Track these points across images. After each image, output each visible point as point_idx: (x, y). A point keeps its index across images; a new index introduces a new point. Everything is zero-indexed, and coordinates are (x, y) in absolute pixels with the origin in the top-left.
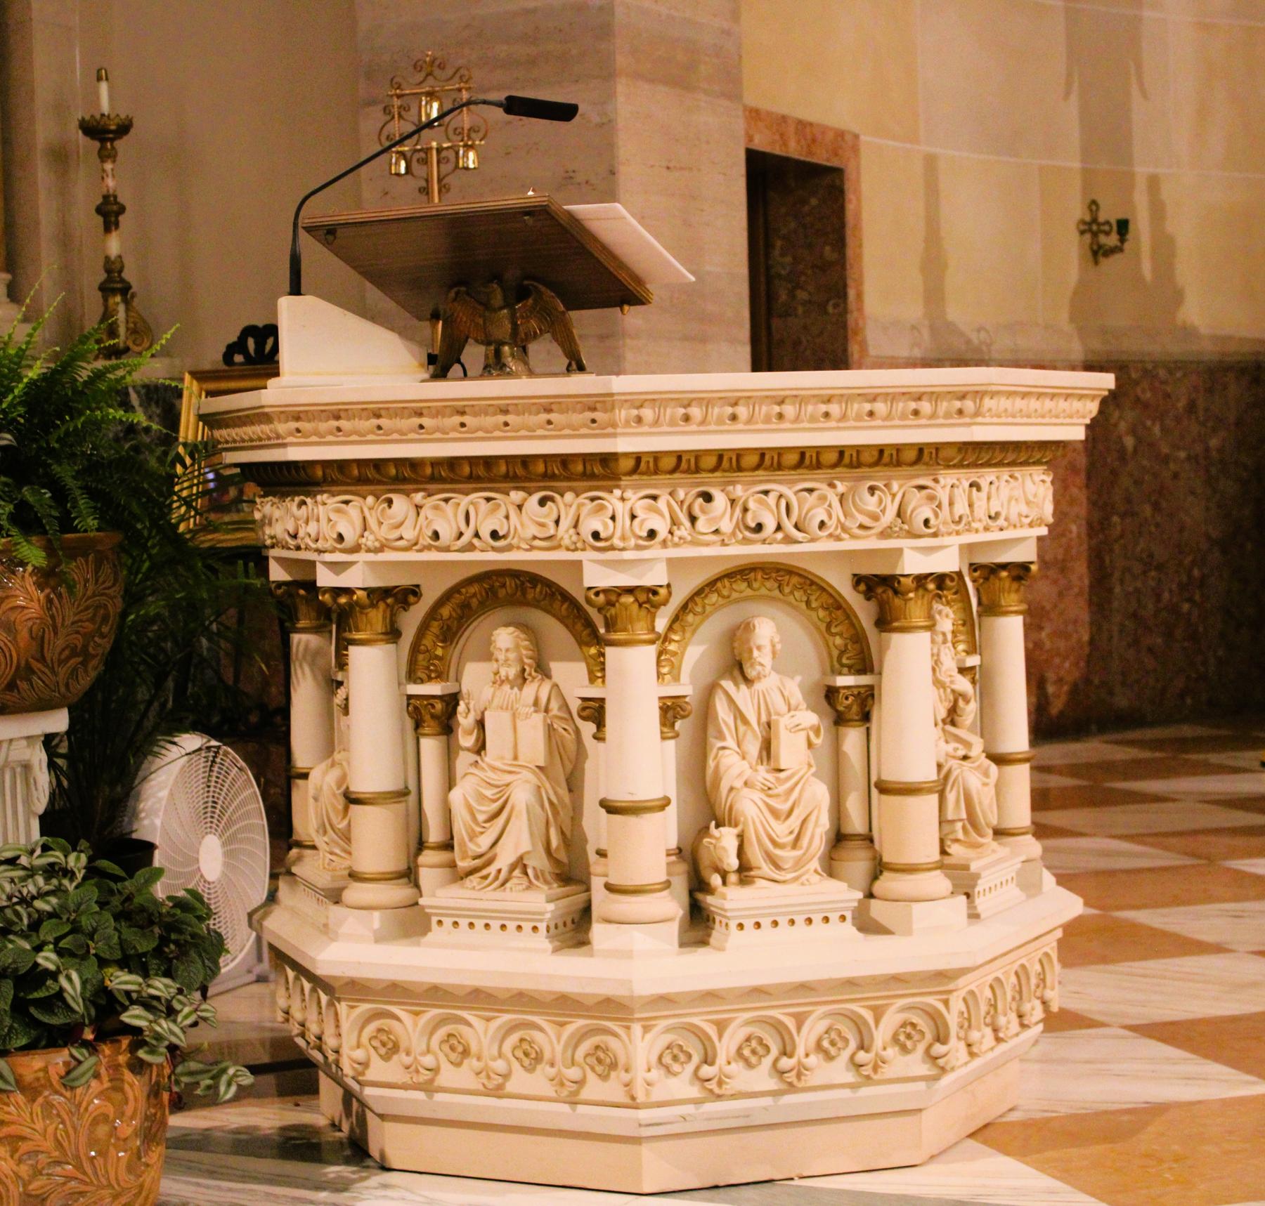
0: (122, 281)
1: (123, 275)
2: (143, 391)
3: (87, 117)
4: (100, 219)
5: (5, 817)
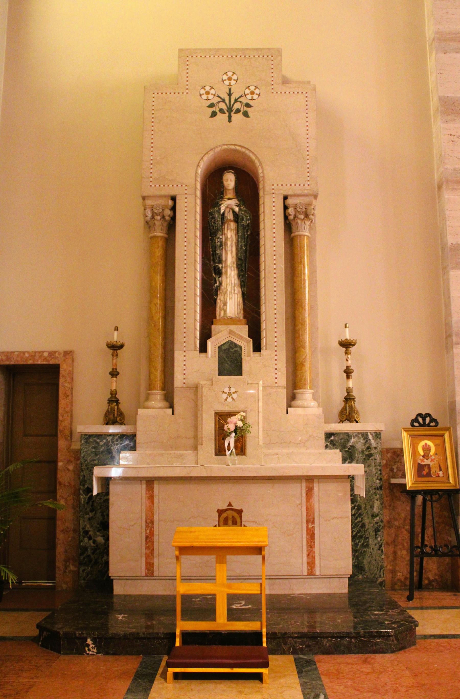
0: (116, 398)
1: (117, 396)
2: (374, 434)
3: (109, 342)
4: (345, 374)
5: (274, 576)
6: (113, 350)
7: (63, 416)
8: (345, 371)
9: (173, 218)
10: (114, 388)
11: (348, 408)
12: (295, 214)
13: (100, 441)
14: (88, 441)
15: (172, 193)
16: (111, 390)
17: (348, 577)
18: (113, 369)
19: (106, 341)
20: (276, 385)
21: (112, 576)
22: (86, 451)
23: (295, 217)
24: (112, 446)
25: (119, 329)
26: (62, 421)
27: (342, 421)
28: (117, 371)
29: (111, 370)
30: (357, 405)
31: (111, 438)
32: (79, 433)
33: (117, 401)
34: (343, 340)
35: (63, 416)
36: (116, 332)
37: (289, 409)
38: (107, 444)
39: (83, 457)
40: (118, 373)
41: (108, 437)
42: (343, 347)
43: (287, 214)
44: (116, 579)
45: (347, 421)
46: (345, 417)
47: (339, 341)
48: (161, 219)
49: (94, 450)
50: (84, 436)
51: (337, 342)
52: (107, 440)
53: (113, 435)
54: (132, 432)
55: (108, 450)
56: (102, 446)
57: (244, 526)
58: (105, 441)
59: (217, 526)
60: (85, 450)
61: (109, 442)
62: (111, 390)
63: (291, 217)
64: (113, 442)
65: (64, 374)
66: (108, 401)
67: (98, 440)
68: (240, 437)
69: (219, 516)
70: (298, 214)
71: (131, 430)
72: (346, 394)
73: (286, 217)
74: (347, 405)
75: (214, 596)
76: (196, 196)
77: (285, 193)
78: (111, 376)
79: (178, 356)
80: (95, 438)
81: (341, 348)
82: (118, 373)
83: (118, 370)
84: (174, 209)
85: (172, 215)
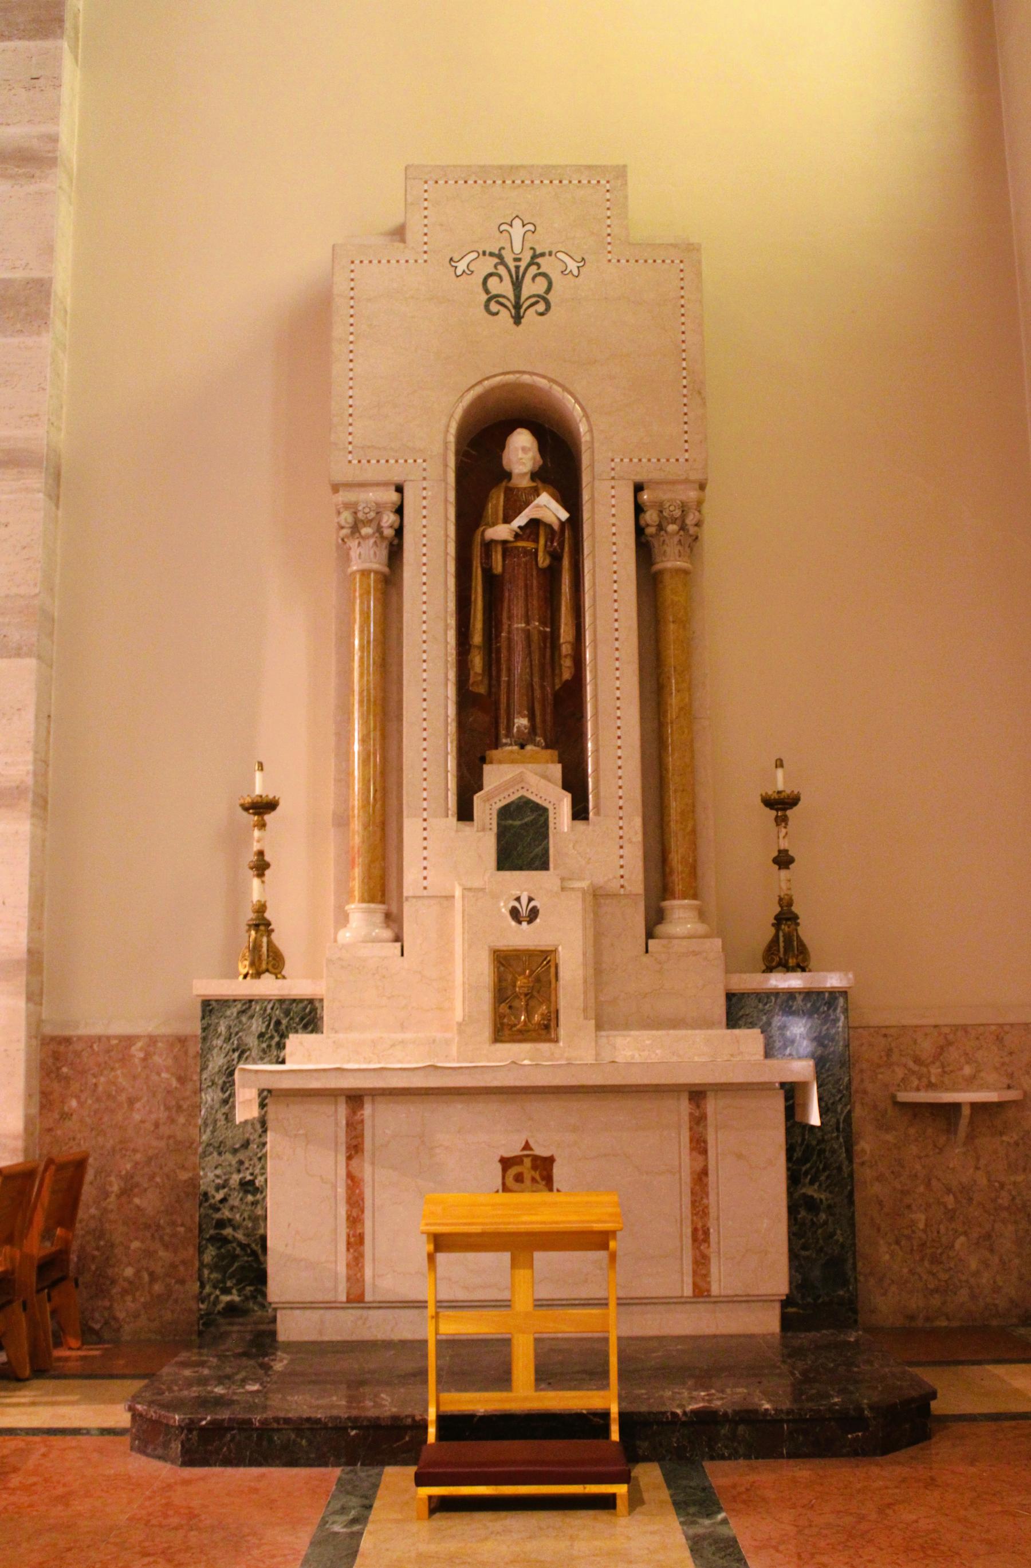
8: (267, 866)
9: (399, 532)
11: (781, 939)
12: (660, 522)
15: (397, 479)
16: (779, 896)
17: (782, 1301)
19: (759, 793)
20: (622, 891)
23: (660, 527)
25: (784, 763)
27: (769, 969)
30: (807, 931)
32: (198, 996)
33: (794, 918)
34: (770, 793)
37: (651, 942)
40: (791, 860)
42: (772, 808)
43: (642, 523)
46: (777, 959)
48: (374, 533)
51: (759, 799)
57: (558, 1191)
59: (501, 1190)
63: (651, 530)
66: (799, 921)
68: (281, 1005)
69: (505, 1170)
70: (664, 524)
73: (640, 531)
74: (781, 934)
75: (506, 1343)
76: (447, 483)
77: (639, 478)
78: (777, 867)
79: (412, 829)
81: (767, 810)
82: (791, 860)
84: (400, 511)
85: (396, 525)
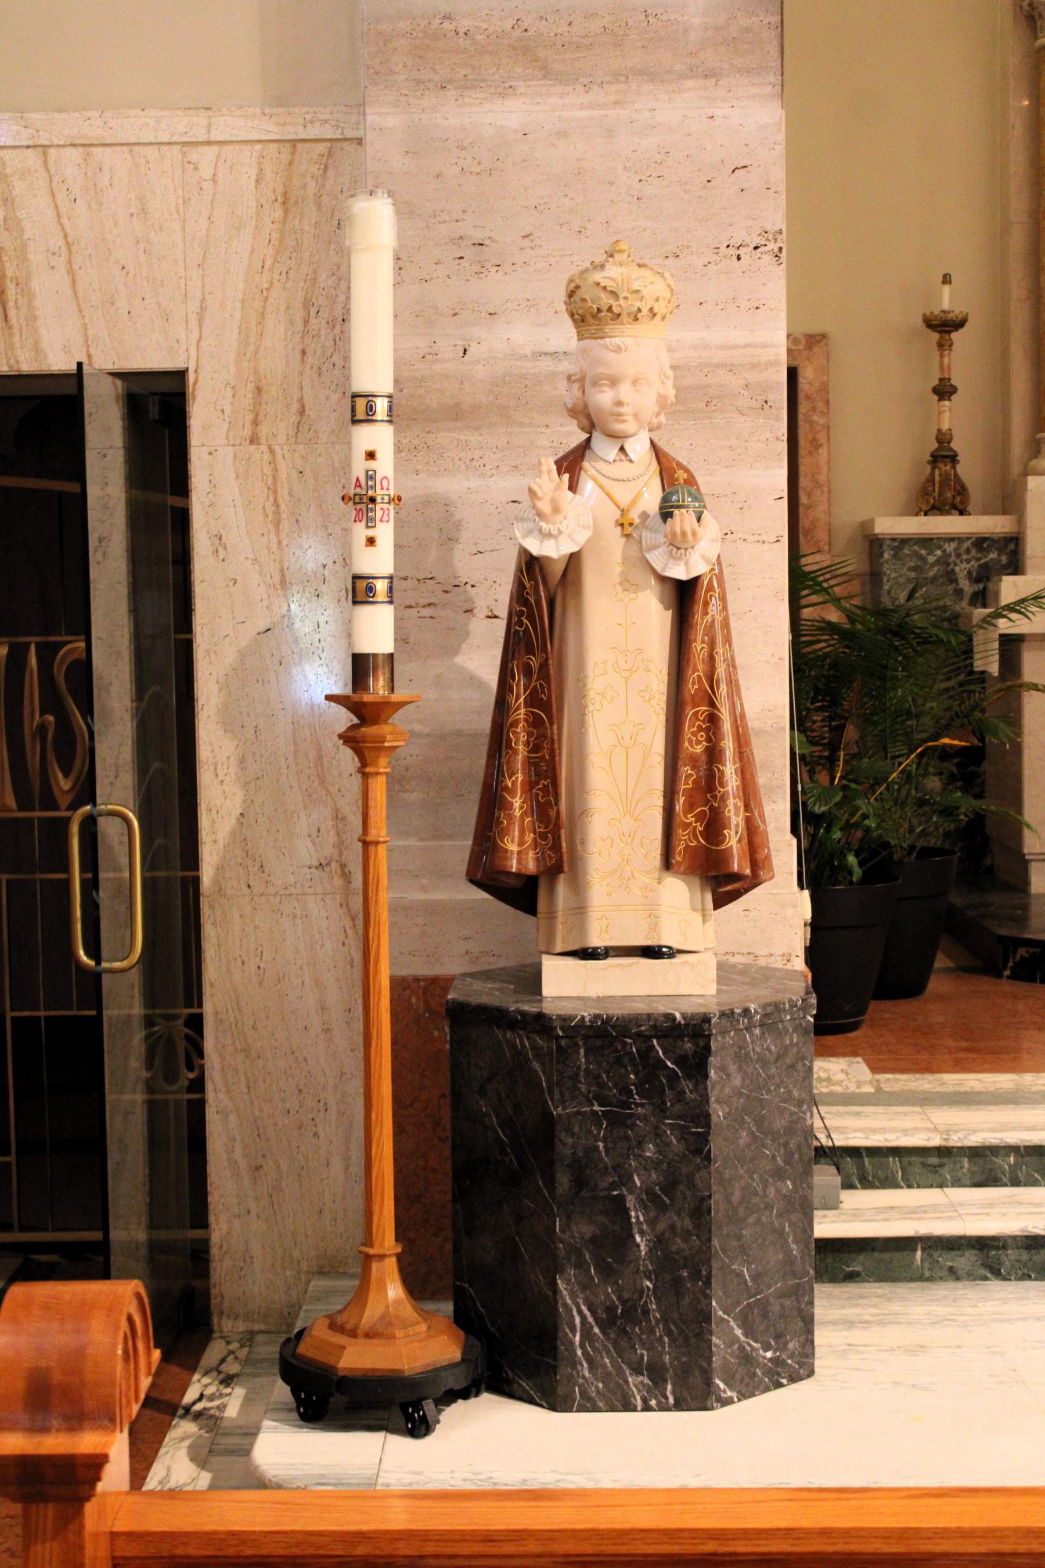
0: (951, 449)
1: (952, 445)
3: (928, 314)
6: (940, 332)
7: (809, 495)
10: (945, 427)
11: (937, 478)
13: (929, 554)
14: (901, 555)
18: (940, 380)
21: (1030, 854)
22: (895, 578)
24: (956, 565)
26: (808, 507)
28: (952, 385)
29: (936, 382)
31: (953, 545)
34: (936, 312)
35: (809, 495)
36: (946, 289)
38: (944, 561)
39: (889, 592)
40: (954, 390)
41: (947, 545)
42: (934, 331)
44: (1039, 860)
45: (935, 511)
47: (924, 316)
49: (913, 575)
50: (888, 542)
52: (944, 551)
53: (959, 539)
54: (1006, 530)
55: (947, 573)
56: (932, 565)
58: (939, 553)
60: (893, 575)
61: (950, 555)
62: (939, 430)
64: (958, 555)
65: (809, 393)
67: (923, 552)
71: (1003, 526)
72: (936, 445)
74: (937, 472)
78: (936, 397)
80: (916, 548)
82: (954, 390)
83: (953, 382)
